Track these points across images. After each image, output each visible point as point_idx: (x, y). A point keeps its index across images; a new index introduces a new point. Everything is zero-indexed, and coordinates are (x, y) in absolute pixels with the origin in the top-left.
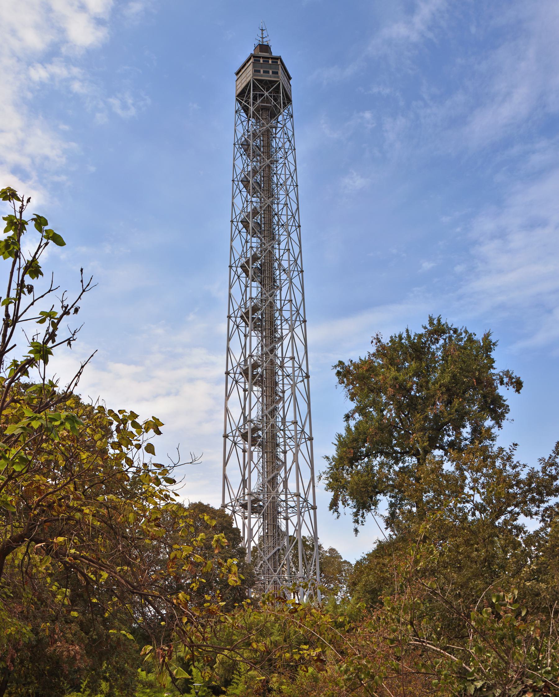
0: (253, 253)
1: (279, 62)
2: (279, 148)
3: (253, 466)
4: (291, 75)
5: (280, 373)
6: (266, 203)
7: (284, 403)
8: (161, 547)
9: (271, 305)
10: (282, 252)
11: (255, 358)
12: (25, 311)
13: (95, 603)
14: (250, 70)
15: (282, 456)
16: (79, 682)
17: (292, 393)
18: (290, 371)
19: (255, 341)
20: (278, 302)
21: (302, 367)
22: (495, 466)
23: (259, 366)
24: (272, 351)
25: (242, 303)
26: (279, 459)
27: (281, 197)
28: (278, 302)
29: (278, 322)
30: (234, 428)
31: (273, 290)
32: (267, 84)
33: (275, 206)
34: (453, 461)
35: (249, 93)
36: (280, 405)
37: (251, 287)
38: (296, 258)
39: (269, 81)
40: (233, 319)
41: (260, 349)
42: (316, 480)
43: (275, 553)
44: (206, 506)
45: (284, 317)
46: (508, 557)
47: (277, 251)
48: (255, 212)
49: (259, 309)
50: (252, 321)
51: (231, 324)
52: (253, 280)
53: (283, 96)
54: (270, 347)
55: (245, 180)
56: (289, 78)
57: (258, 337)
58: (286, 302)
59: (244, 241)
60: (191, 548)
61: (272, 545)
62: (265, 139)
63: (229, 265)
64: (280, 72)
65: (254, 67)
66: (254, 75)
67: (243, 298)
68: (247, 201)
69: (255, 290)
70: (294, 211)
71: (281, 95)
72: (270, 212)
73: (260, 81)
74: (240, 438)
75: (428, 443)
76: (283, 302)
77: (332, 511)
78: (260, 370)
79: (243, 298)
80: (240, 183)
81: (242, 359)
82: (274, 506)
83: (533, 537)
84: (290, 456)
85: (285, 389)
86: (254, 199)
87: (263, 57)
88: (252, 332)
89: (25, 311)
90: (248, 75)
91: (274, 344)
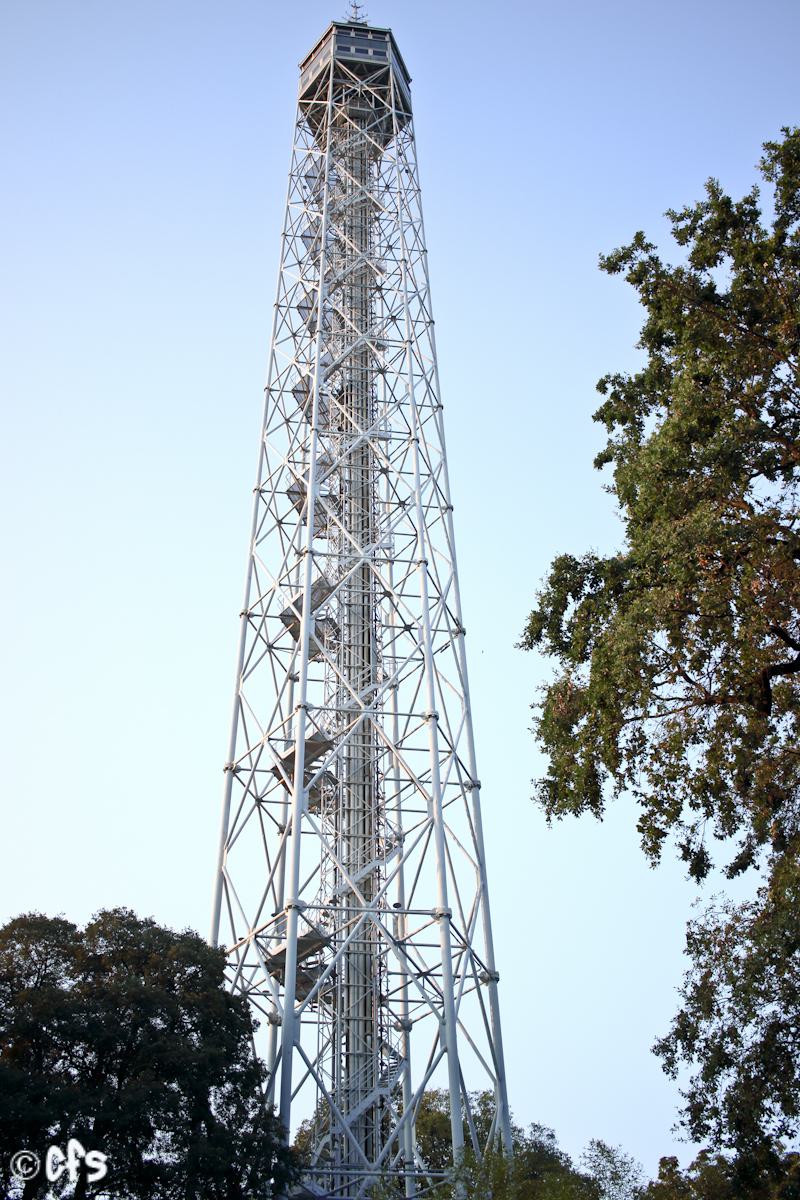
0: (315, 576)
1: (387, 38)
2: (402, 504)
3: (299, 1068)
4: (411, 76)
5: (393, 962)
6: (356, 559)
7: (403, 858)
8: (59, 1025)
9: (367, 732)
10: (384, 250)
11: (314, 916)
12: (306, 884)
13: (594, 669)
14: (331, 46)
15: (395, 1039)
16: (108, 967)
17: (424, 517)
18: (432, 958)
19: (312, 850)
20: (388, 721)
21: (459, 752)
22: (587, 1179)
23: (326, 942)
24: (367, 886)
25: (277, 722)
26: (384, 1045)
27: (400, 543)
28: (388, 721)
29: (389, 789)
30: (243, 932)
31: (372, 686)
32: (363, 70)
33: (383, 571)
34: (183, 1144)
35: (328, 77)
36: (392, 865)
37: (300, 832)
38: (443, 590)
39: (367, 65)
40: (244, 776)
41: (330, 877)
42: (294, 471)
43: (369, 1112)
44: (182, 937)
45: (408, 771)
46: (713, 782)
47: (389, 720)
48: (322, 590)
49: (329, 745)
50: (306, 782)
51: (238, 790)
52: (313, 654)
53: (395, 93)
54: (362, 873)
55: (297, 489)
56: (408, 80)
57: (322, 835)
58: (415, 722)
59: (282, 676)
60: (347, 462)
61: (361, 1086)
62: (356, 476)
63: (225, 761)
64: (390, 53)
65: (337, 41)
66: (336, 53)
67: (271, 882)
68: (299, 554)
69: (321, 682)
70: (434, 465)
71: (392, 87)
72: (365, 459)
73: (350, 65)
74: (262, 973)
75: (772, 400)
76: (402, 720)
77: (623, 808)
78: (328, 956)
79: (271, 882)
80: (299, 240)
81: (270, 907)
82: (367, 968)
83: (748, 280)
84: (425, 1033)
85: (412, 1017)
86: (321, 545)
87: (356, 30)
88: (304, 820)
89: (306, 884)
90: (327, 58)
91: (374, 864)
